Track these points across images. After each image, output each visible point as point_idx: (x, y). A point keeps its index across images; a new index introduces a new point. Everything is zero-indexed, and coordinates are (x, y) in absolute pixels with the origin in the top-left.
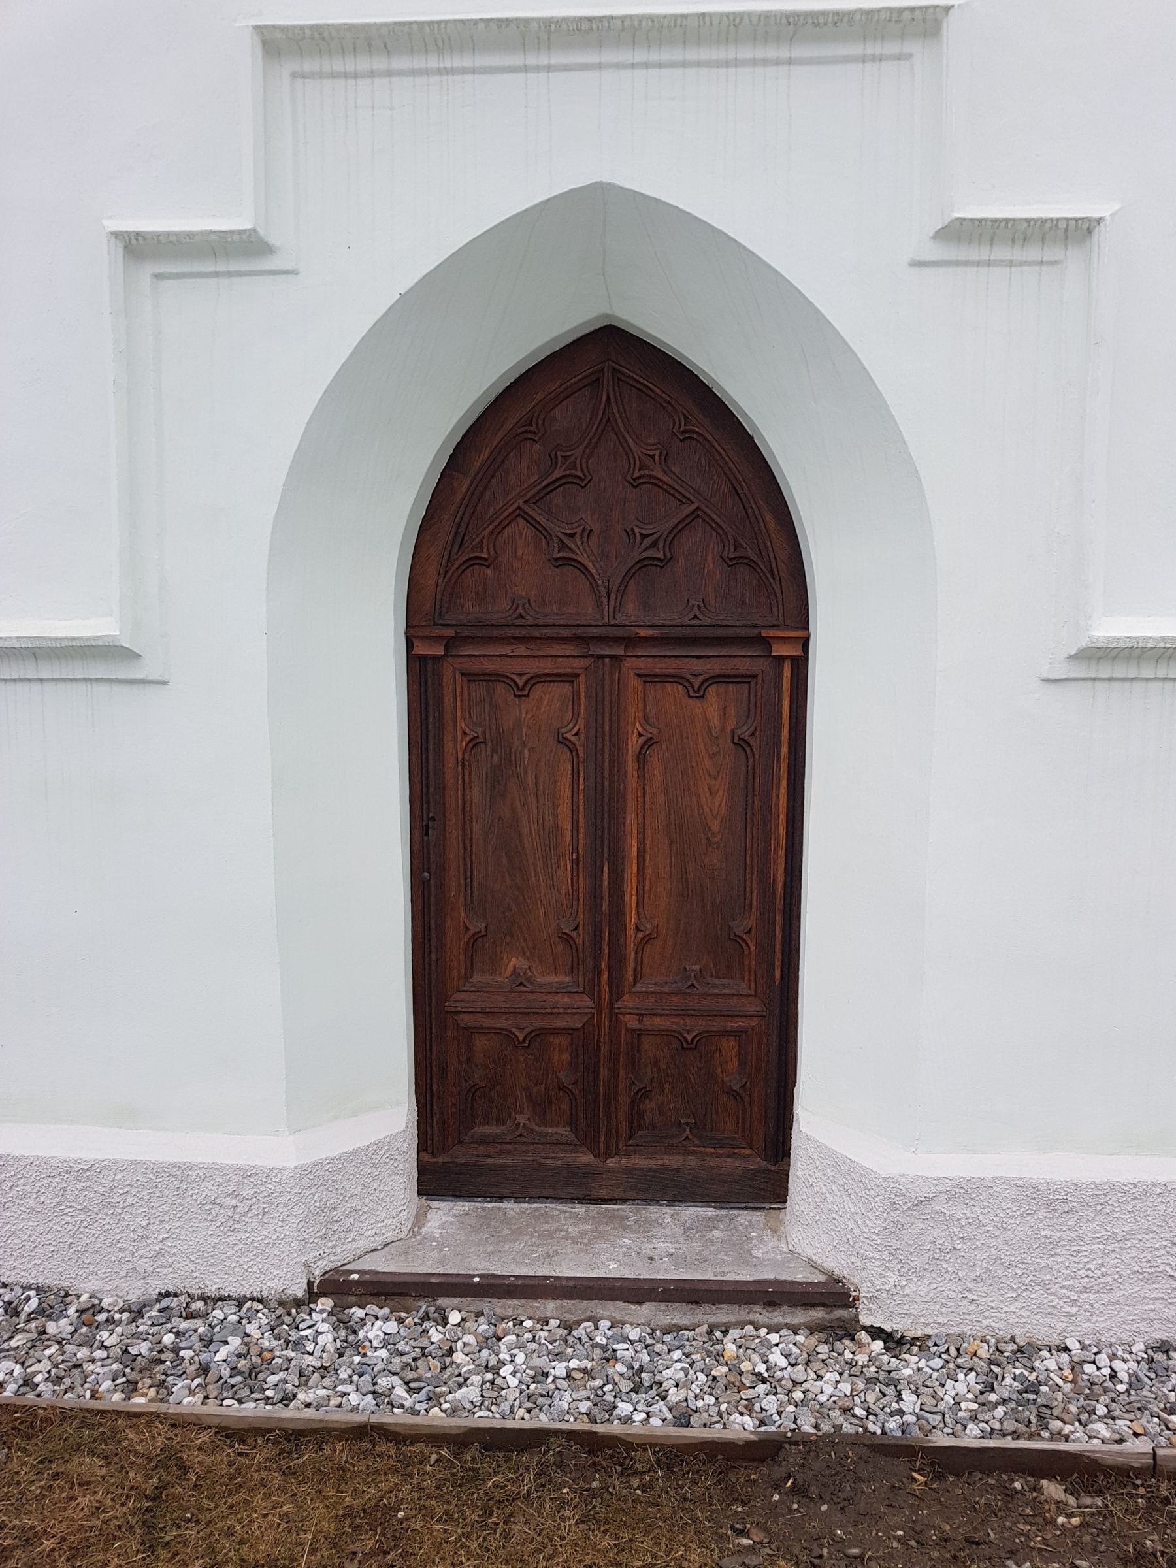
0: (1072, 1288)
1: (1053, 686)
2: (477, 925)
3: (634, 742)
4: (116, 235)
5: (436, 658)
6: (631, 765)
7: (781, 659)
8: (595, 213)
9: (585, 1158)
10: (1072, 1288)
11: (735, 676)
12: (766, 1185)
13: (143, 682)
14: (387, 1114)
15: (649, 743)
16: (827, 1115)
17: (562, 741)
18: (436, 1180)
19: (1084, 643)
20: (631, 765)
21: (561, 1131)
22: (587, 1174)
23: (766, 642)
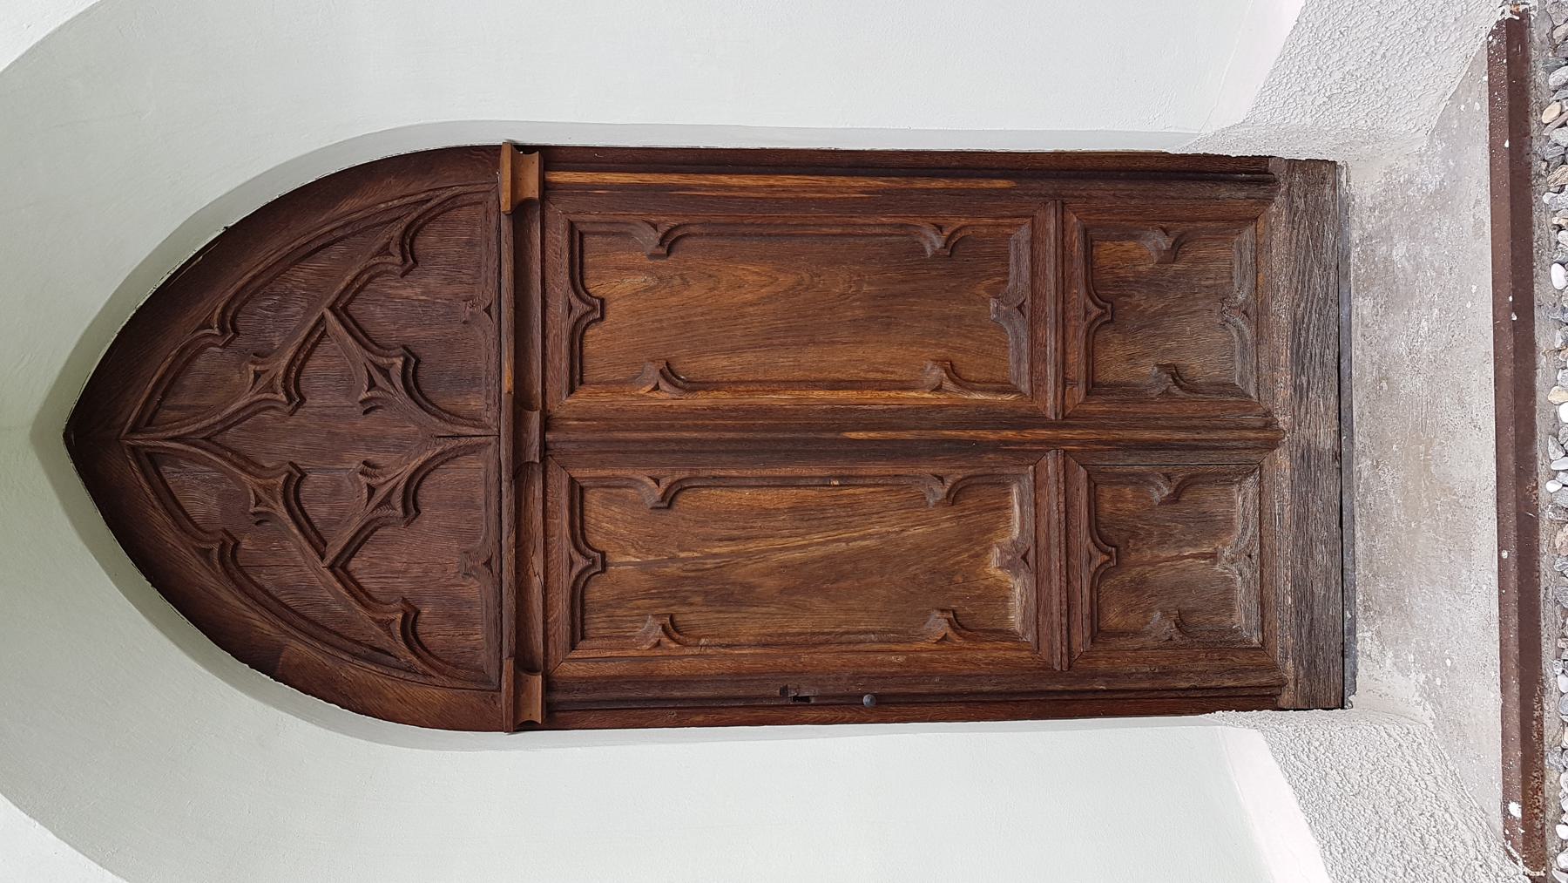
2: (938, 625)
3: (667, 396)
5: (548, 686)
6: (702, 400)
7: (545, 186)
9: (1282, 460)
15: (669, 374)
20: (702, 400)
21: (1242, 498)
22: (1306, 458)
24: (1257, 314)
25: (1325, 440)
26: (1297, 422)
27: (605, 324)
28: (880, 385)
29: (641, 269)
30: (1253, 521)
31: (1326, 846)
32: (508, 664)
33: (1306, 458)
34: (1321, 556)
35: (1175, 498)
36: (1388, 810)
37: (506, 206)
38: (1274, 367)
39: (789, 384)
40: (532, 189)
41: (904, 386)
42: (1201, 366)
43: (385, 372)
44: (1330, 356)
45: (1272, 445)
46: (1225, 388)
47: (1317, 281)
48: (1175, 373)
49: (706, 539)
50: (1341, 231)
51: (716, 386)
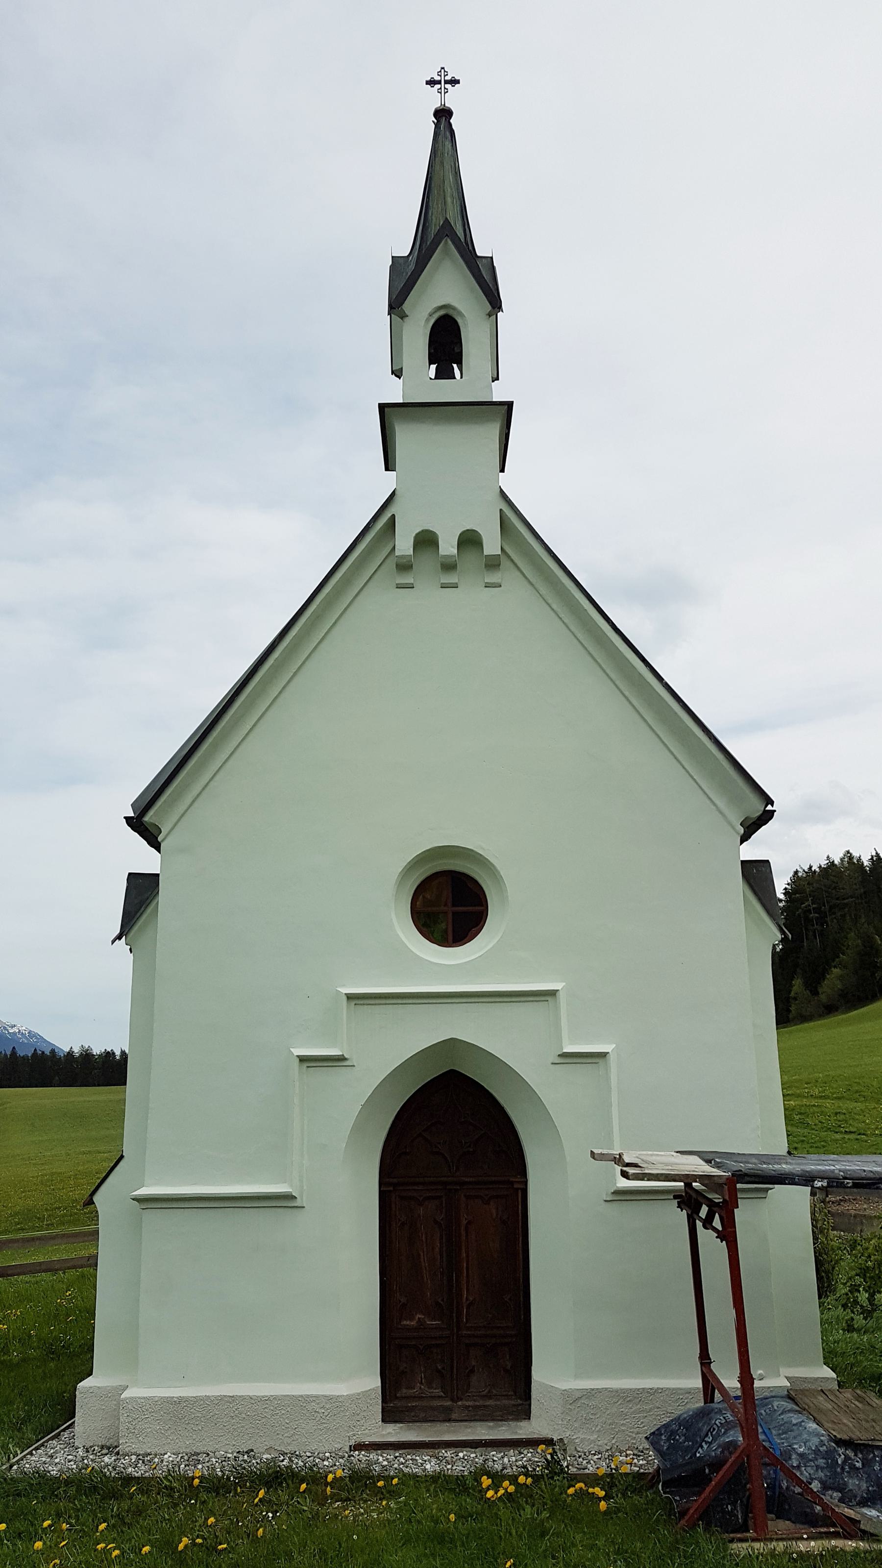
0: (632, 1432)
1: (607, 1203)
2: (403, 1300)
3: (465, 1222)
4: (298, 1056)
5: (390, 1191)
6: (463, 1233)
7: (517, 1189)
8: (451, 1045)
9: (449, 1403)
10: (632, 1432)
11: (428, 197)
12: (525, 1413)
13: (297, 1207)
14: (370, 1382)
15: (469, 1223)
16: (543, 1373)
17: (436, 1222)
18: (388, 1416)
19: (615, 1188)
20: (463, 1233)
21: (438, 1392)
22: (449, 1410)
23: (512, 1183)
24: (489, 1397)
25: (454, 1416)
26: (459, 1407)
27: (272, 1443)
28: (468, 1282)
29: (497, 1215)
30: (433, 1395)
31: (359, 1394)
32: (395, 1180)
33: (449, 1410)
34: (422, 1415)
35: (438, 1371)
36: (365, 1414)
37: (511, 1179)
38: (475, 1401)
39: (467, 1256)
40: (516, 1186)
41: (468, 1290)
42: (474, 1379)
43: (470, 1146)
44: (477, 1418)
45: (452, 1400)
46: (469, 1385)
47: (498, 1413)
48: (472, 1371)
49: (426, 1234)
50: (512, 1420)
51: (467, 1236)
